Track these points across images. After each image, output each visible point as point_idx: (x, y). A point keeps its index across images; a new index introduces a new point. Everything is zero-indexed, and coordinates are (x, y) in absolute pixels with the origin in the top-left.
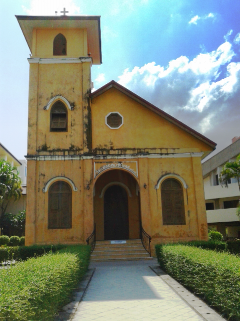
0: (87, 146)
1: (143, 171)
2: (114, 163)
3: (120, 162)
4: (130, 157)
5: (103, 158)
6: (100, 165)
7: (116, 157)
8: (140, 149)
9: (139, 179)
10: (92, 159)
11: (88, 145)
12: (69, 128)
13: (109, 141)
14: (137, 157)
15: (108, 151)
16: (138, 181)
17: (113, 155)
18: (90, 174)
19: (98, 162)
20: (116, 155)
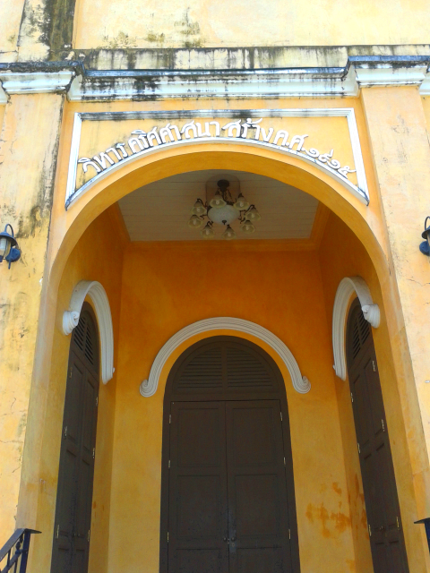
0: (38, 33)
1: (402, 156)
2: (203, 119)
3: (244, 115)
4: (308, 87)
5: (132, 92)
6: (110, 130)
7: (218, 88)
8: (369, 47)
9: (374, 201)
10: (63, 92)
11: (47, 28)
12: (234, 205)
13: (179, 17)
14: (348, 87)
15: (169, 54)
16: (369, 217)
17: (193, 75)
18: (35, 175)
19: (97, 117)
20: (216, 74)
